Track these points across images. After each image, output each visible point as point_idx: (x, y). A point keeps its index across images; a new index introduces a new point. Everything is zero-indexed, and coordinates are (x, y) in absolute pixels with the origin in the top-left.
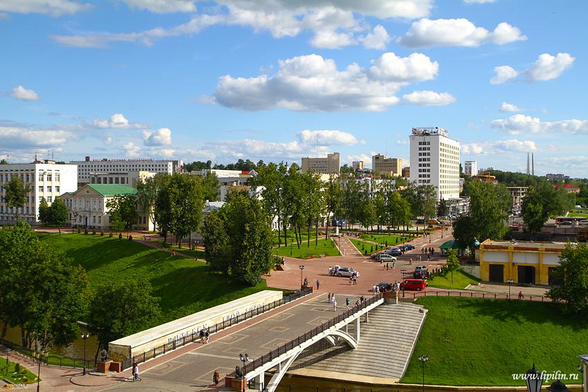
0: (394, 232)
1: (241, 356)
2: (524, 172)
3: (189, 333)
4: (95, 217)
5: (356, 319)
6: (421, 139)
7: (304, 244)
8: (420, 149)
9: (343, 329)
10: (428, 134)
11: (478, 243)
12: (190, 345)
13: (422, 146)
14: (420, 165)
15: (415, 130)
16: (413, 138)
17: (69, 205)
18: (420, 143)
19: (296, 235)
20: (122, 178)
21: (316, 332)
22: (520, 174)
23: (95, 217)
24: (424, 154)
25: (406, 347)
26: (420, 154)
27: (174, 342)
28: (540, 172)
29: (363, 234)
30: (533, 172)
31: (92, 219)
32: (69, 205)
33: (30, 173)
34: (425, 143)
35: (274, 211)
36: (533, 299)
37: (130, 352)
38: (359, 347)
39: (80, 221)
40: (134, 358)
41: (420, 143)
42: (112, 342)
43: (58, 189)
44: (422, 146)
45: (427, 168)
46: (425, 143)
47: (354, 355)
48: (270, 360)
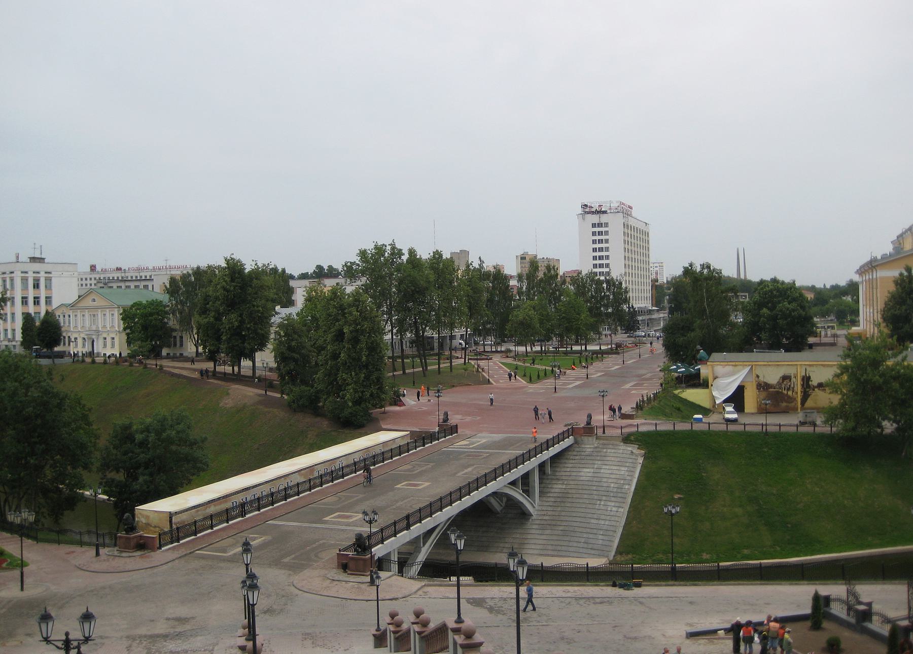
0: (566, 353)
1: (365, 513)
2: (735, 276)
3: (282, 487)
4: (105, 339)
5: (534, 467)
6: (595, 219)
7: (433, 371)
8: (594, 242)
9: (513, 483)
10: (605, 212)
11: (611, 297)
12: (295, 500)
13: (597, 229)
14: (594, 242)
15: (586, 205)
16: (583, 219)
17: (67, 324)
18: (594, 225)
19: (421, 361)
20: (10, 277)
21: (469, 488)
22: (729, 277)
23: (105, 339)
24: (601, 241)
25: (614, 509)
26: (594, 250)
27: (243, 505)
28: (754, 276)
29: (517, 356)
30: (745, 276)
31: (101, 341)
32: (67, 324)
33: (7, 276)
34: (600, 225)
35: (424, 324)
36: (783, 429)
37: (171, 521)
38: (539, 513)
39: (84, 346)
40: (178, 528)
41: (594, 225)
42: (137, 508)
43: (48, 300)
44: (597, 229)
45: (603, 245)
46: (600, 225)
47: (533, 527)
48: (408, 527)
